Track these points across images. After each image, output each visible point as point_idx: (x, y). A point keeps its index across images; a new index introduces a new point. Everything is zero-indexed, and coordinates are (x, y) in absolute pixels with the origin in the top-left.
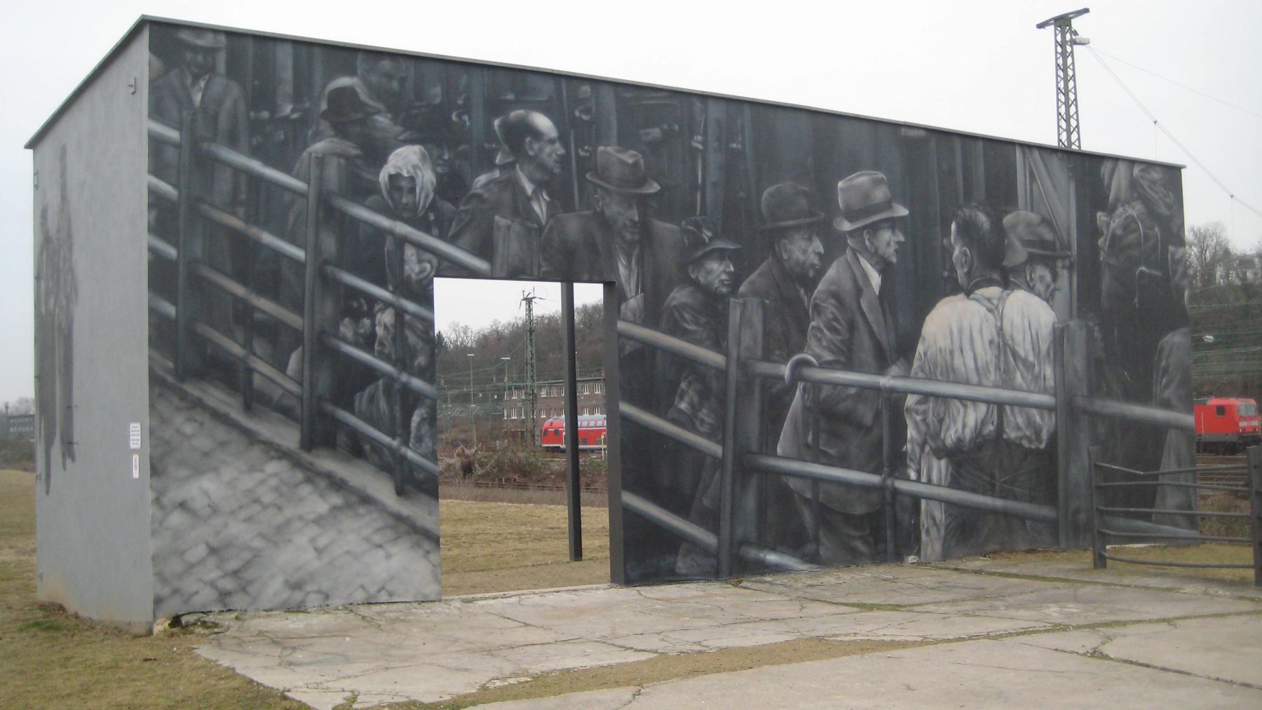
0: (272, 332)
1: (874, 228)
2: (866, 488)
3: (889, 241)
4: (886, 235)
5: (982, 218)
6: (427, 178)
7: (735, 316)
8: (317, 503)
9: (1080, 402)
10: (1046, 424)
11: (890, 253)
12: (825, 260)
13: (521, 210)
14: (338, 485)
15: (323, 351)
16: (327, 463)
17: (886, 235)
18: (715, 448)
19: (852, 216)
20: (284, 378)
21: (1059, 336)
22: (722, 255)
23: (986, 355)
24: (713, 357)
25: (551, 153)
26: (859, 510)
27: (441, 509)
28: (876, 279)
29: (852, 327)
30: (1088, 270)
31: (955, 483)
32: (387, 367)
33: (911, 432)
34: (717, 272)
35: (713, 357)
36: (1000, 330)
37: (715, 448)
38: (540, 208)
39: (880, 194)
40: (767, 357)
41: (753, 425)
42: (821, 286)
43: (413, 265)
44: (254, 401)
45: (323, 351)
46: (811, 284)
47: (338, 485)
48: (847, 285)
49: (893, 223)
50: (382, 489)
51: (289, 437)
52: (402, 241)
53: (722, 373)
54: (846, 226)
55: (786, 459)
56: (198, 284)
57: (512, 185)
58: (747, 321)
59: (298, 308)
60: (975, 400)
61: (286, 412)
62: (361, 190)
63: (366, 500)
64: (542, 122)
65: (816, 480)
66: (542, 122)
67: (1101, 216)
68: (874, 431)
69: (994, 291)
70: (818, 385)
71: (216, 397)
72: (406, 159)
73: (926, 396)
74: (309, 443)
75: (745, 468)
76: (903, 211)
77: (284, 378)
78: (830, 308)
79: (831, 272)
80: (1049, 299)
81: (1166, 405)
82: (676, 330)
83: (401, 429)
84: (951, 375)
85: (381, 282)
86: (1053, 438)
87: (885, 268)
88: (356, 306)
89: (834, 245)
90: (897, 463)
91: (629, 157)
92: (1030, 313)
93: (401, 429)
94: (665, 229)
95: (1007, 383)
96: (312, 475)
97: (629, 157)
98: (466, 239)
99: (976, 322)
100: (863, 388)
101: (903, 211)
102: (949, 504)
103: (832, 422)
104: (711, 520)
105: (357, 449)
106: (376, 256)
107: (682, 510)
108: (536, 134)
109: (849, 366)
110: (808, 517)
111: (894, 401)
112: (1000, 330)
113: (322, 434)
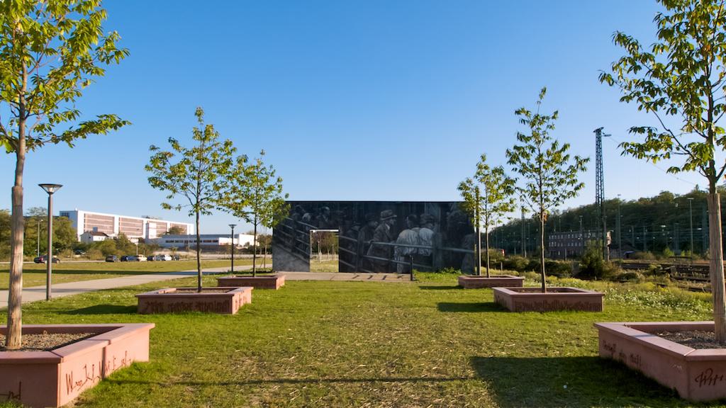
0: (288, 237)
1: (389, 219)
2: (386, 261)
3: (392, 221)
4: (391, 220)
5: (415, 216)
6: (309, 217)
7: (359, 235)
8: (292, 259)
9: (440, 247)
10: (430, 252)
11: (393, 223)
12: (378, 225)
13: (323, 220)
14: (296, 256)
15: (294, 240)
16: (295, 254)
17: (391, 220)
18: (355, 254)
19: (383, 217)
20: (289, 243)
21: (434, 237)
22: (358, 225)
23: (414, 239)
24: (356, 240)
25: (328, 213)
26: (383, 264)
27: (457, 281)
28: (389, 228)
29: (383, 235)
30: (443, 223)
31: (405, 261)
32: (303, 242)
33: (395, 252)
34: (357, 228)
35: (356, 240)
36: (418, 235)
37: (355, 254)
38: (326, 220)
39: (391, 213)
40: (365, 240)
41: (362, 250)
42: (377, 229)
43: (307, 229)
44: (285, 246)
45: (294, 240)
46: (375, 229)
47: (296, 256)
48: (382, 229)
49: (393, 218)
50: (302, 258)
51: (290, 251)
52: (306, 226)
53: (356, 243)
54: (383, 219)
55: (369, 256)
56: (278, 232)
57: (322, 217)
58: (362, 235)
59: (291, 234)
60: (411, 247)
61: (289, 247)
62: (300, 219)
63: (300, 259)
64: (327, 208)
65: (375, 259)
66: (327, 208)
67: (448, 213)
68: (390, 252)
69: (417, 228)
70: (376, 244)
71: (281, 246)
72: (306, 215)
73: (399, 246)
74: (292, 251)
75: (360, 257)
76: (395, 216)
77: (289, 243)
78: (378, 233)
79: (379, 227)
80: (432, 229)
81: (466, 249)
82: (349, 236)
83: (305, 250)
84: (405, 243)
85: (302, 231)
86: (431, 254)
87: (391, 226)
88: (299, 234)
89: (380, 223)
90: (392, 257)
91: (341, 212)
92: (426, 232)
93: (305, 250)
94: (347, 222)
95: (420, 244)
96: (293, 255)
97: (341, 212)
98: (695, 211)
99: (412, 234)
100: (385, 245)
101: (395, 216)
102: (403, 264)
103: (378, 250)
104: (354, 264)
105: (299, 252)
106: (302, 228)
107: (349, 262)
108: (326, 210)
109: (382, 241)
110: (373, 265)
111: (392, 248)
112: (418, 235)
113: (294, 250)
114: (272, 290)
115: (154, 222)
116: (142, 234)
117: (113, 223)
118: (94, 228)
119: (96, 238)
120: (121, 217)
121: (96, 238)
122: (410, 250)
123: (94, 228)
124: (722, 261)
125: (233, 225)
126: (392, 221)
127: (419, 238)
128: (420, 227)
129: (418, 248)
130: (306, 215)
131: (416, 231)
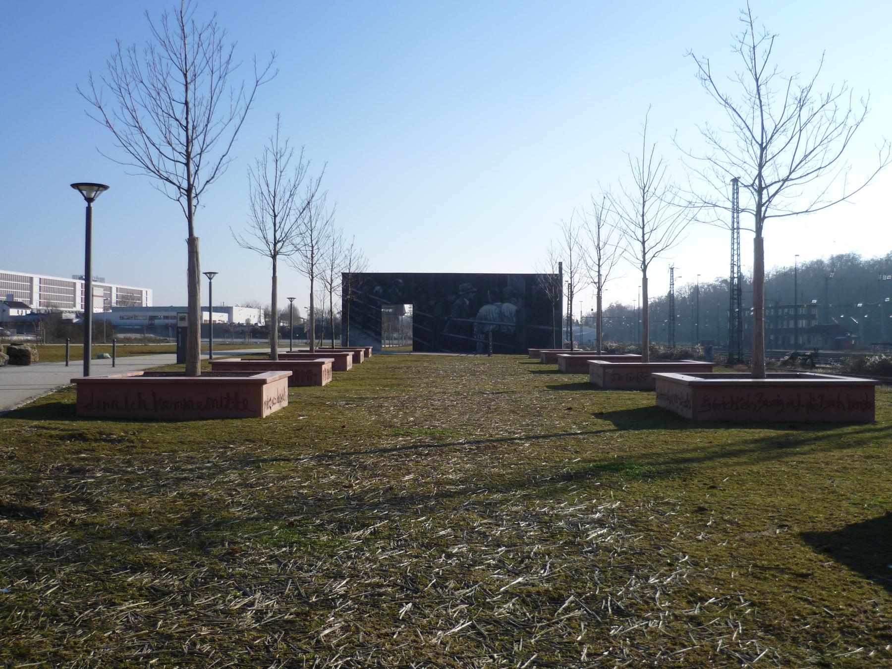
21: (517, 312)
28: (468, 302)
38: (400, 294)
50: (373, 335)
72: (378, 288)
80: (515, 304)
87: (470, 300)
92: (509, 307)
114: (317, 388)
115: (101, 287)
116: (74, 306)
117: (31, 288)
118: (8, 296)
119: (13, 312)
120: (119, 286)
121: (13, 312)
122: (491, 327)
123: (8, 296)
124: (200, 340)
125: (210, 273)
126: (471, 295)
127: (501, 314)
128: (503, 301)
129: (500, 325)
130: (378, 288)
131: (498, 306)
